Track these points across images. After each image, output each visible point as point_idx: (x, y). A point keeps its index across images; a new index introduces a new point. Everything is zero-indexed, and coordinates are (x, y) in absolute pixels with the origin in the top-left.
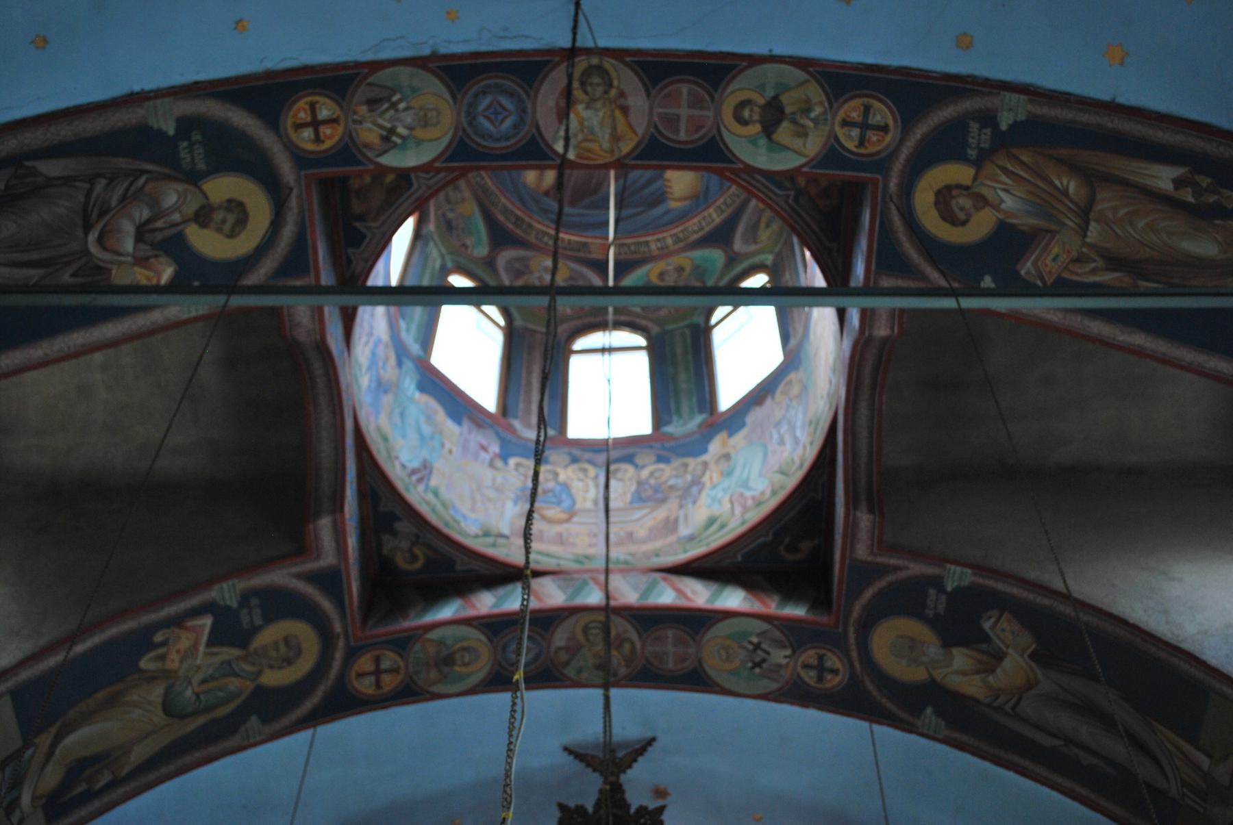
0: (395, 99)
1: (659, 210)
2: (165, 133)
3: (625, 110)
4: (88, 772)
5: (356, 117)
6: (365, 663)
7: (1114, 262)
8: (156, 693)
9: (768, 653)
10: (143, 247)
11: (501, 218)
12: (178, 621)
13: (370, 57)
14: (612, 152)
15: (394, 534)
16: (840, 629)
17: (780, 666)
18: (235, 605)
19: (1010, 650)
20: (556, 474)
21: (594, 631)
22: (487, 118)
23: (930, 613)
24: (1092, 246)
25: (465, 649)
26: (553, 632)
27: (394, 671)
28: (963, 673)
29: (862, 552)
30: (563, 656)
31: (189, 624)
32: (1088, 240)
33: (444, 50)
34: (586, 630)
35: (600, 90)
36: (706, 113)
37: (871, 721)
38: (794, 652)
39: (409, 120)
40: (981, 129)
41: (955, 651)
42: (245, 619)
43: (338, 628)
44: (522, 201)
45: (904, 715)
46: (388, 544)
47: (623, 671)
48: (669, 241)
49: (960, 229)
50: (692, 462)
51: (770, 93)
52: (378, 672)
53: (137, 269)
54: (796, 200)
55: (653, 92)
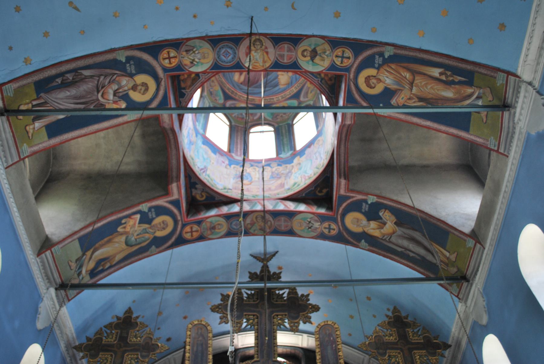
0: (194, 50)
1: (277, 88)
3: (267, 53)
4: (103, 263)
6: (188, 229)
8: (123, 238)
11: (227, 91)
12: (129, 216)
13: (186, 36)
14: (263, 66)
15: (196, 189)
17: (317, 228)
19: (388, 222)
23: (363, 211)
24: (414, 94)
25: (219, 224)
28: (374, 229)
29: (342, 192)
33: (210, 34)
34: (256, 218)
35: (259, 46)
37: (346, 245)
43: (179, 218)
45: (355, 243)
46: (194, 192)
48: (280, 98)
51: (313, 47)
54: (321, 81)
55: (276, 47)
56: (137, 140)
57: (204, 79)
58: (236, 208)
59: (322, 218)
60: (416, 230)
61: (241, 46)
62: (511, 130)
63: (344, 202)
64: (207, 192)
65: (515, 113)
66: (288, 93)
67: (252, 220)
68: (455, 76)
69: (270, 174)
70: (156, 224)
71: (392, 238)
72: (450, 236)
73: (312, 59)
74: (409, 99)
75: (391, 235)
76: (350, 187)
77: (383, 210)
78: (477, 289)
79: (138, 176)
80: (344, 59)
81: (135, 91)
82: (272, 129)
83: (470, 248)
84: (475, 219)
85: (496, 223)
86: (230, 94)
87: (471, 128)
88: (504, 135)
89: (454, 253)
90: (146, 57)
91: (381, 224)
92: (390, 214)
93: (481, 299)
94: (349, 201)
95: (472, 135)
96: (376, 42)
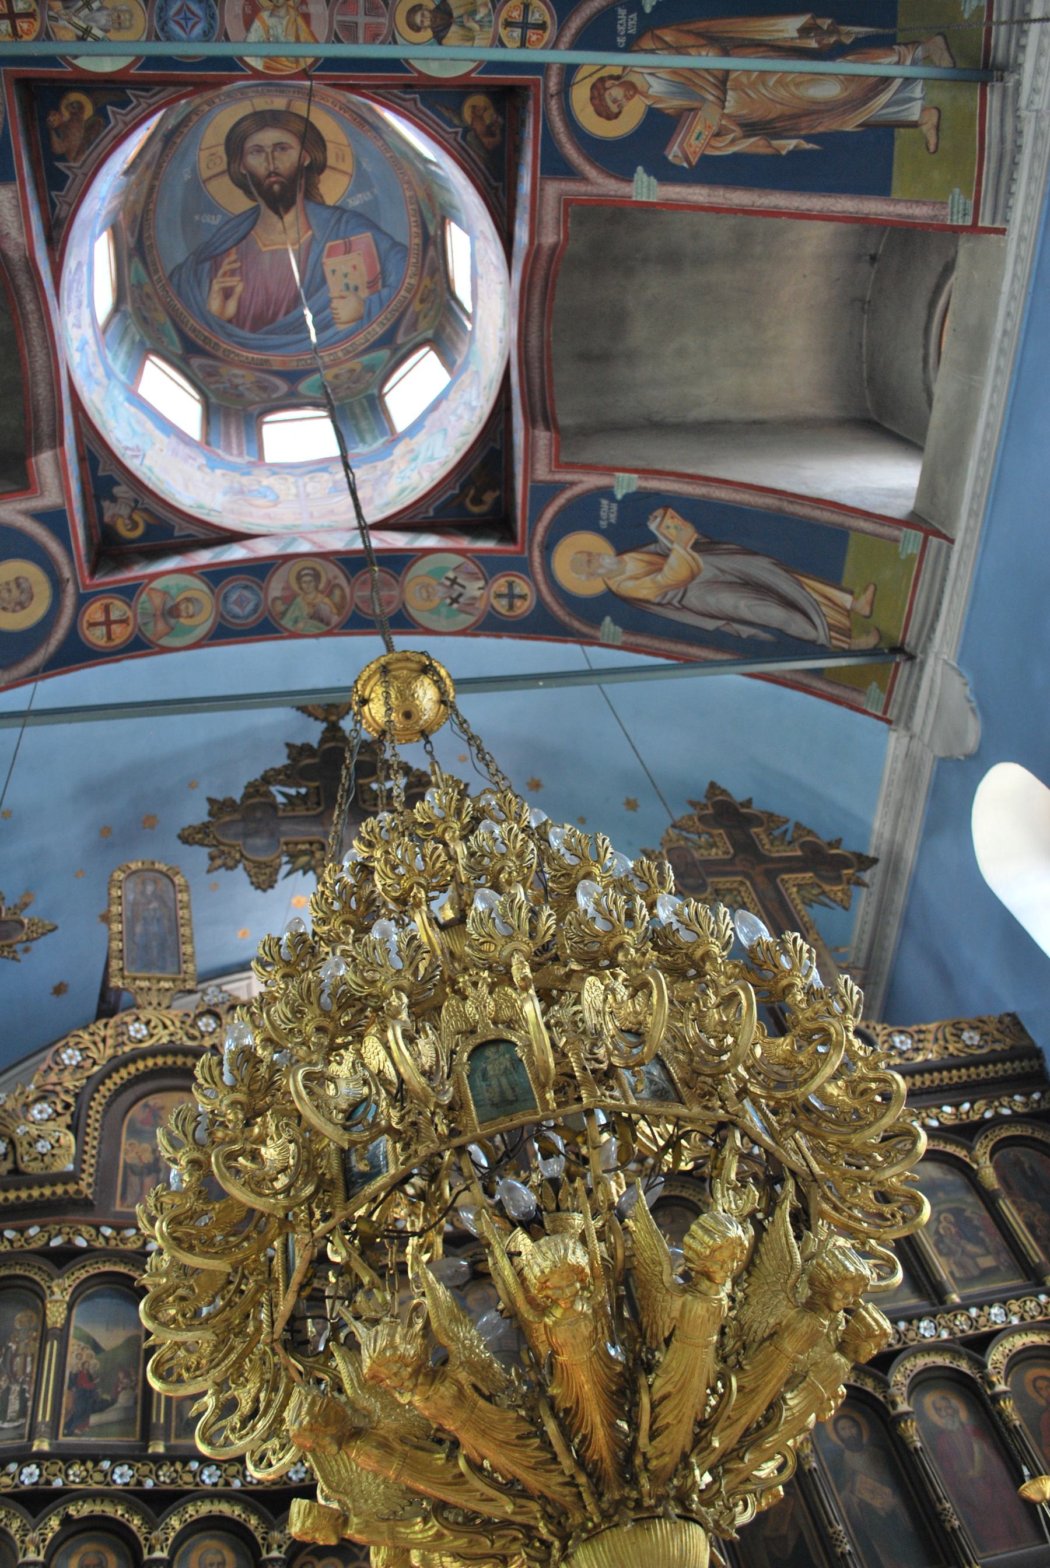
3: (307, 18)
5: (51, 13)
6: (94, 612)
7: (750, 128)
9: (464, 587)
11: (192, 335)
15: (114, 499)
16: (526, 554)
17: (474, 598)
19: (676, 546)
20: (260, 482)
21: (308, 578)
22: (178, 23)
23: (603, 524)
24: (729, 117)
25: (188, 600)
26: (269, 582)
27: (123, 621)
28: (635, 578)
29: (542, 473)
30: (280, 607)
32: (726, 111)
34: (299, 578)
36: (381, 20)
38: (487, 582)
40: (628, 13)
41: (627, 557)
43: (67, 573)
44: (210, 326)
45: (585, 629)
47: (335, 619)
48: (340, 354)
50: (380, 465)
52: (108, 623)
54: (464, 137)
57: (121, 125)
58: (236, 553)
60: (755, 553)
62: (1009, 145)
63: (548, 505)
64: (146, 510)
65: (1018, 84)
66: (361, 340)
67: (287, 587)
69: (330, 485)
71: (689, 594)
72: (851, 543)
73: (439, 37)
74: (718, 135)
75: (684, 586)
76: (564, 458)
77: (659, 512)
80: (529, 32)
82: (324, 414)
83: (910, 558)
84: (914, 493)
85: (984, 441)
86: (200, 343)
87: (895, 183)
88: (989, 167)
89: (866, 589)
92: (678, 521)
93: (957, 682)
94: (561, 500)
95: (899, 201)
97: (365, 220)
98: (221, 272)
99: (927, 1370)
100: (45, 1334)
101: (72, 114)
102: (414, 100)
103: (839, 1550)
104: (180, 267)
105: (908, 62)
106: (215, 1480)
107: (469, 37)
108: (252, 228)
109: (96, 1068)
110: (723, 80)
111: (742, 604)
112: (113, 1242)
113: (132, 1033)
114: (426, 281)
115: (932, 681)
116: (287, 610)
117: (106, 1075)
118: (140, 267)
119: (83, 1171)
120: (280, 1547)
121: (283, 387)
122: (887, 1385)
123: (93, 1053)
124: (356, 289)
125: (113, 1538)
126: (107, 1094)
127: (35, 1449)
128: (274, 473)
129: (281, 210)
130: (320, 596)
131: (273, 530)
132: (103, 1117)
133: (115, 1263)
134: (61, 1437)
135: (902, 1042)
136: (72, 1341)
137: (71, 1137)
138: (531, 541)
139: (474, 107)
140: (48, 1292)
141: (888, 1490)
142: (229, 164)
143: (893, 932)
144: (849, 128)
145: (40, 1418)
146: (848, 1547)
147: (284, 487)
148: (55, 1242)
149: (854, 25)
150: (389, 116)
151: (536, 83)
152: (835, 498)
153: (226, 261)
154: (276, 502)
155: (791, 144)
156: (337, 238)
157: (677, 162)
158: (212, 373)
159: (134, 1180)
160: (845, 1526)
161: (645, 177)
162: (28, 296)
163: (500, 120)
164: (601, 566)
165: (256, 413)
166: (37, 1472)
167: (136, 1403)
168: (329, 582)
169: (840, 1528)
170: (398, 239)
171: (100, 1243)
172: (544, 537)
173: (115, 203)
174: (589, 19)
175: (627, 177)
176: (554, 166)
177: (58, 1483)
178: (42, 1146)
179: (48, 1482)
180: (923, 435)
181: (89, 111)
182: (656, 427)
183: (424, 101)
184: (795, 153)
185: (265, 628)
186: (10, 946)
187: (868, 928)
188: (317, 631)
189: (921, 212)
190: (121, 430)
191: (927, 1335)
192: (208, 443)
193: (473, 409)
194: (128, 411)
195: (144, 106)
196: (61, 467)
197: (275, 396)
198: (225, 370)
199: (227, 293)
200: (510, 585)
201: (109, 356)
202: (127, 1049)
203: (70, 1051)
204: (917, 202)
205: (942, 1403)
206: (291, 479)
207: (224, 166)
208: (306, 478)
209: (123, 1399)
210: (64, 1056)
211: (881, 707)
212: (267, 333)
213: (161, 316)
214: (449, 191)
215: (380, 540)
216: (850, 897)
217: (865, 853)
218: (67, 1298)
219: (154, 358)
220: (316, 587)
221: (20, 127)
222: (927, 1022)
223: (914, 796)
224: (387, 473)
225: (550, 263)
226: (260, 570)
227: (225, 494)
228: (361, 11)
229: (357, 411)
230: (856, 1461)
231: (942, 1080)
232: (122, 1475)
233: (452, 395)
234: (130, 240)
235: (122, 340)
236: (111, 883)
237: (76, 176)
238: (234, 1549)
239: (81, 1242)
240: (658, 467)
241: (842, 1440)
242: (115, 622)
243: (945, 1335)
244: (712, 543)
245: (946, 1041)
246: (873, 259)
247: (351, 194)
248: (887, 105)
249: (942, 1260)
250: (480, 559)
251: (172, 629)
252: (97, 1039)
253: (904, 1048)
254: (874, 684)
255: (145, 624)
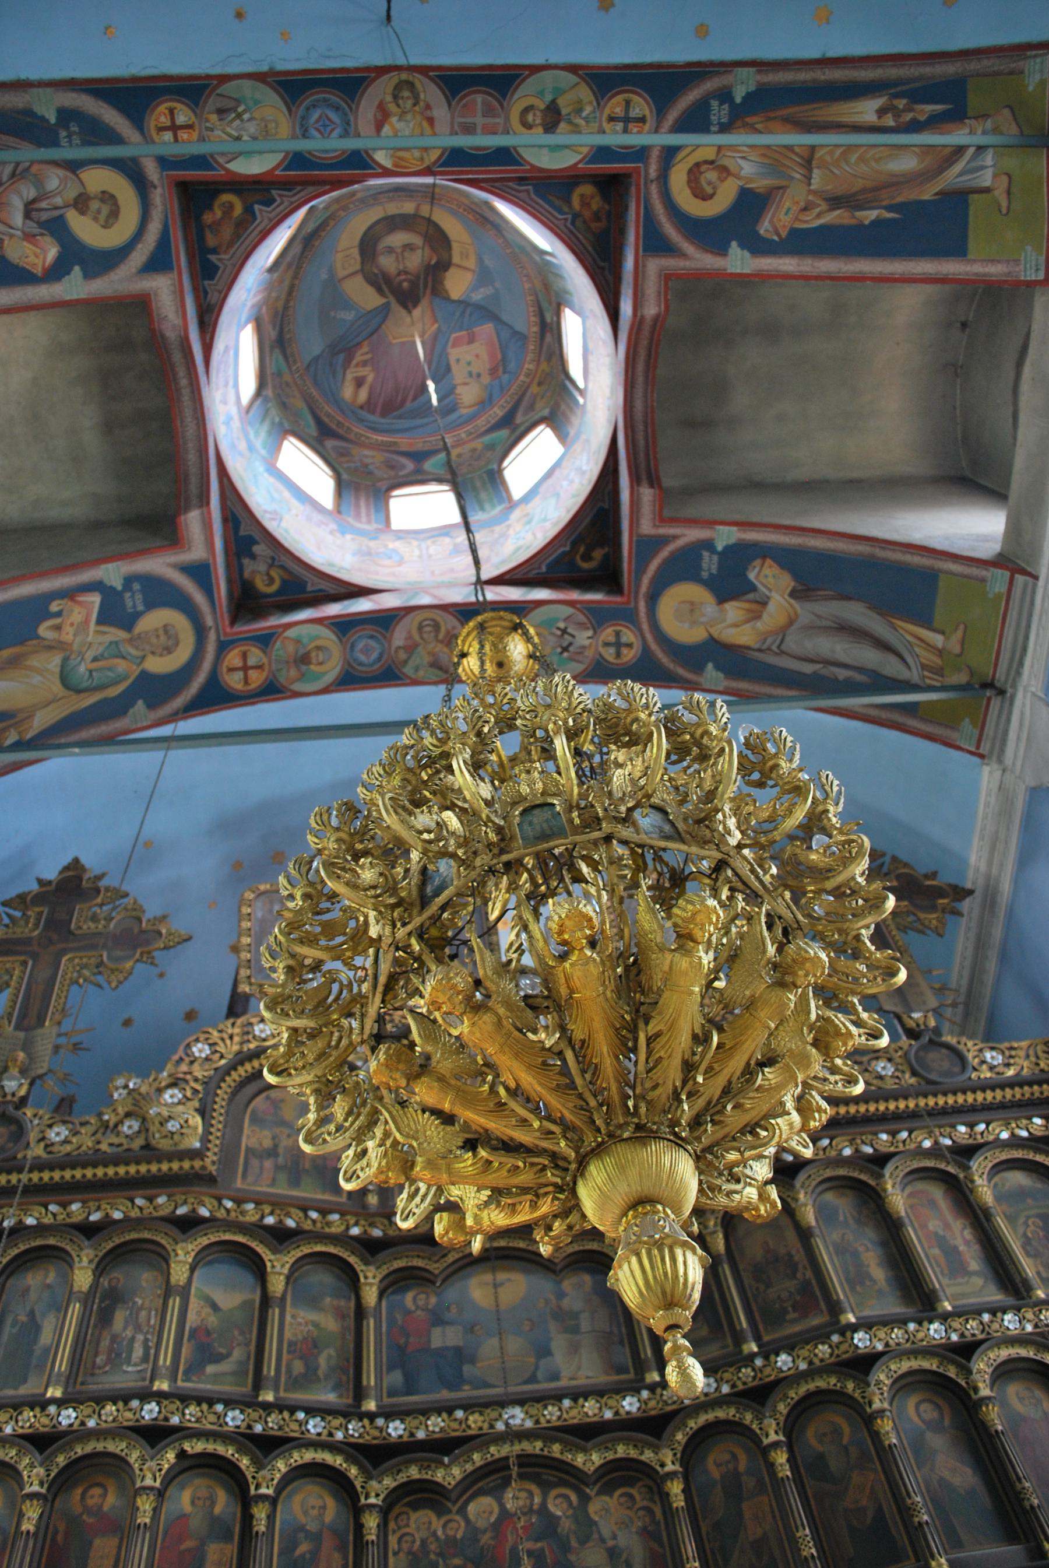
0: (240, 109)
1: (453, 417)
2: (47, 121)
3: (431, 121)
6: (233, 658)
7: (835, 202)
8: (54, 662)
9: (573, 636)
10: (29, 223)
11: (326, 420)
12: (70, 594)
13: (217, 71)
14: (422, 159)
15: (253, 557)
16: (632, 605)
17: (584, 647)
18: (120, 588)
20: (386, 546)
22: (320, 117)
23: (705, 575)
24: (815, 192)
25: (319, 648)
27: (259, 667)
28: (736, 625)
29: (647, 527)
30: (402, 655)
31: (80, 599)
33: (281, 67)
34: (420, 628)
35: (410, 103)
36: (497, 120)
38: (595, 632)
39: (252, 130)
40: (721, 104)
41: (728, 606)
42: (129, 603)
43: (209, 621)
44: (343, 412)
46: (249, 567)
48: (463, 436)
49: (709, 202)
50: (497, 529)
51: (549, 98)
52: (245, 668)
53: (25, 243)
54: (573, 223)
55: (453, 103)
56: (92, 441)
57: (266, 221)
58: (363, 605)
59: (597, 617)
60: (849, 598)
61: (363, 103)
63: (653, 557)
66: (482, 423)
67: (409, 637)
68: (916, 107)
69: (451, 547)
70: (146, 633)
71: (788, 639)
72: (941, 584)
74: (805, 209)
75: (782, 632)
76: (666, 513)
77: (758, 562)
78: (1029, 695)
79: (96, 526)
81: (83, 213)
82: (446, 488)
83: (998, 596)
86: (334, 427)
87: (971, 245)
89: (956, 629)
90: (111, 117)
91: (754, 606)
94: (665, 553)
95: (975, 261)
96: (712, 64)
97: (486, 312)
98: (354, 362)
99: (1010, 1361)
100: (168, 1291)
101: (224, 213)
102: (527, 191)
103: (916, 1520)
104: (317, 359)
105: (979, 131)
106: (319, 1430)
107: (576, 130)
108: (383, 321)
109: (223, 1062)
110: (808, 159)
111: (838, 648)
112: (233, 1214)
113: (257, 1033)
114: (544, 366)
115: (1022, 714)
116: (409, 658)
117: (233, 1067)
118: (281, 358)
119: (208, 1149)
120: (377, 1495)
121: (410, 465)
122: (970, 1372)
123: (221, 1048)
124: (479, 375)
125: (223, 1475)
126: (233, 1084)
127: (155, 1388)
128: (400, 538)
129: (410, 306)
130: (440, 645)
131: (397, 586)
132: (228, 1104)
133: (235, 1233)
134: (180, 1383)
135: (993, 1058)
136: (193, 1299)
137: (199, 1120)
138: (637, 593)
139: (582, 196)
140: (172, 1254)
141: (969, 1471)
142: (362, 263)
143: (992, 966)
144: (926, 197)
145: (161, 1362)
146: (925, 1518)
147: (409, 550)
148: (181, 1211)
149: (928, 103)
150: (504, 208)
151: (637, 171)
152: (925, 543)
153: (359, 352)
154: (401, 562)
155: (873, 214)
156: (461, 329)
157: (768, 236)
158: (344, 454)
159: (255, 1162)
160: (923, 1498)
161: (739, 251)
162: (181, 372)
163: (607, 207)
164: (704, 615)
165: (384, 488)
166: (157, 1409)
167: (249, 1358)
168: (448, 632)
169: (919, 1499)
170: (518, 328)
171: (221, 1214)
172: (648, 588)
173: (259, 297)
174: (684, 112)
175: (722, 251)
176: (655, 243)
177: (175, 1420)
178: (172, 1126)
179: (166, 1419)
180: (1007, 484)
181: (238, 210)
182: (756, 486)
183: (536, 192)
184: (877, 223)
185: (389, 675)
186: (149, 953)
187: (968, 963)
188: (435, 679)
189: (996, 270)
190: (261, 496)
191: (1011, 1327)
192: (339, 512)
193: (583, 473)
194: (267, 480)
195: (286, 204)
196: (207, 525)
197: (401, 473)
198: (356, 451)
199: (359, 382)
200: (618, 634)
201: (252, 433)
202: (252, 1046)
203: (200, 1045)
204: (992, 261)
205: (1026, 1394)
206: (415, 543)
207: (358, 267)
208: (429, 542)
209: (237, 1354)
210: (194, 1049)
211: (974, 741)
212: (395, 418)
213: (302, 400)
214: (561, 277)
215: (493, 594)
216: (944, 925)
217: (961, 885)
218: (190, 1260)
219: (292, 439)
220: (436, 636)
221: (179, 223)
222: (1020, 1040)
223: (1008, 829)
224: (504, 535)
225: (652, 332)
226: (385, 620)
227: (354, 555)
228: (479, 114)
229: (476, 482)
230: (938, 1442)
231: (1032, 1094)
232: (234, 1419)
233: (564, 463)
234: (272, 333)
235: (263, 420)
236: (242, 901)
237: (226, 266)
238: (335, 1495)
239: (204, 1212)
240: (755, 519)
241: (923, 1421)
242: (252, 668)
243: (1029, 1328)
244: (808, 590)
245: (1038, 1057)
246: (964, 325)
247: (474, 289)
248: (961, 174)
249: (1030, 1261)
250: (589, 609)
251: (303, 675)
252: (225, 1036)
253: (995, 1063)
254: (967, 720)
255: (279, 670)
